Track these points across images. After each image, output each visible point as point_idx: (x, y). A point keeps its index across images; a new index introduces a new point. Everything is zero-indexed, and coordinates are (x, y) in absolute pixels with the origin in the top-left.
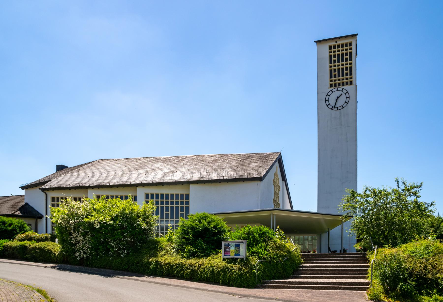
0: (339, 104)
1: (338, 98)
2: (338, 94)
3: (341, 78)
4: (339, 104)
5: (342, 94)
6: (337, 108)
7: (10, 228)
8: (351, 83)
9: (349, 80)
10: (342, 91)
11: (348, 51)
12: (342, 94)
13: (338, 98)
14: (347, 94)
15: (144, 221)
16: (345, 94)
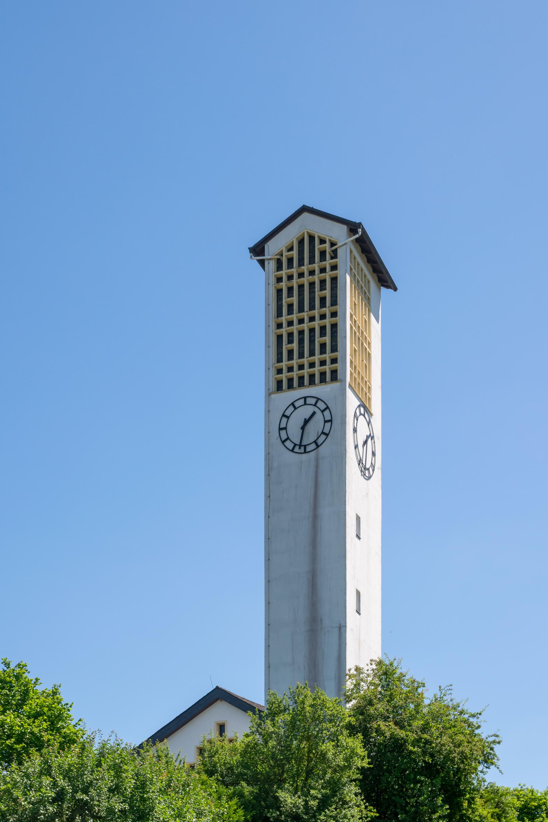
0: (309, 438)
1: (306, 422)
2: (305, 412)
3: (305, 326)
4: (309, 438)
5: (314, 413)
6: (305, 446)
7: (411, 748)
8: (334, 373)
9: (327, 368)
10: (315, 405)
11: (328, 322)
12: (314, 413)
13: (306, 422)
14: (327, 413)
15: (112, 773)
16: (322, 411)
